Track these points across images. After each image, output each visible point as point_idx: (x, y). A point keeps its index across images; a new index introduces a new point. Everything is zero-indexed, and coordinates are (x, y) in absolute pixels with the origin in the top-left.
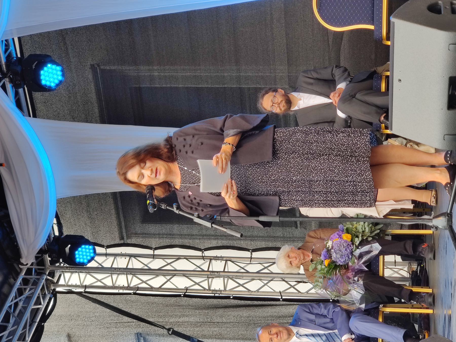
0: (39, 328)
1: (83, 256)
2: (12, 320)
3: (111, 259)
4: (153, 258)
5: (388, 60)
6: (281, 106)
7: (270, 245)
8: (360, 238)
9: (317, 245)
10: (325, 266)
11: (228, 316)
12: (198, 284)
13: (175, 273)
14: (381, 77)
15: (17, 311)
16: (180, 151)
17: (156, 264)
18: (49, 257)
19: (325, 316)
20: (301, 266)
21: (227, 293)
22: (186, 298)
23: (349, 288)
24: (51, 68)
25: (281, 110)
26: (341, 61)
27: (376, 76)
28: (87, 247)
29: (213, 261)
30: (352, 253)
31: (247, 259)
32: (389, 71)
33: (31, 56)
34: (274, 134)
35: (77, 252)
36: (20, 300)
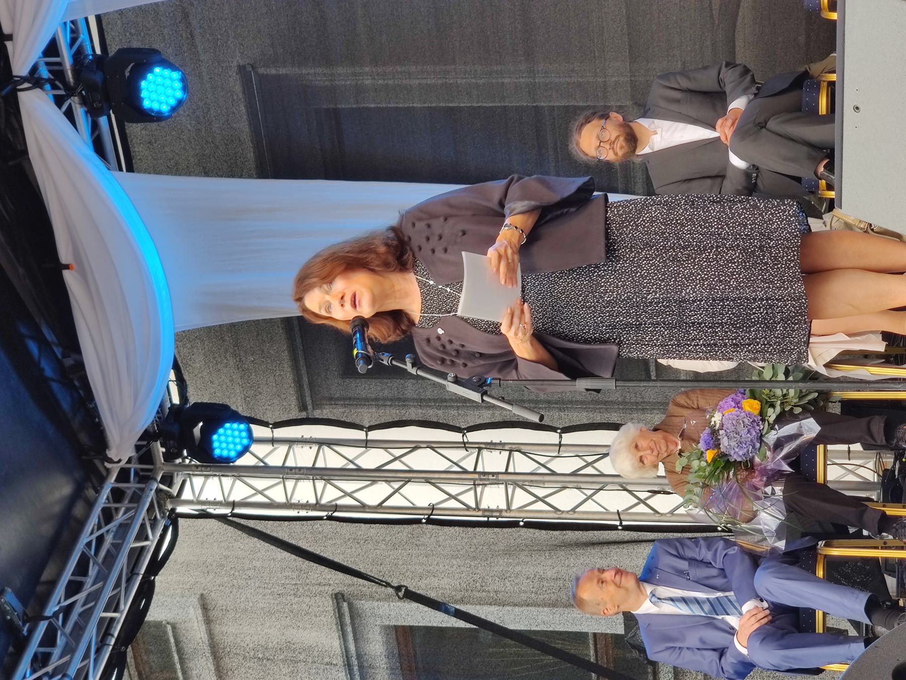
0: (146, 586)
1: (228, 443)
2: (93, 571)
3: (283, 448)
4: (366, 447)
5: (833, 49)
6: (617, 146)
7: (598, 418)
8: (778, 409)
9: (692, 423)
10: (706, 461)
11: (516, 577)
12: (455, 498)
13: (409, 476)
14: (819, 84)
15: (103, 553)
16: (420, 248)
17: (372, 459)
18: (162, 446)
19: (708, 564)
20: (661, 464)
21: (512, 514)
22: (430, 526)
23: (755, 509)
24: (162, 76)
25: (616, 154)
26: (738, 49)
27: (807, 82)
28: (235, 426)
29: (485, 453)
30: (761, 438)
31: (552, 448)
32: (834, 72)
33: (121, 52)
34: (607, 212)
35: (215, 437)
36: (108, 531)
